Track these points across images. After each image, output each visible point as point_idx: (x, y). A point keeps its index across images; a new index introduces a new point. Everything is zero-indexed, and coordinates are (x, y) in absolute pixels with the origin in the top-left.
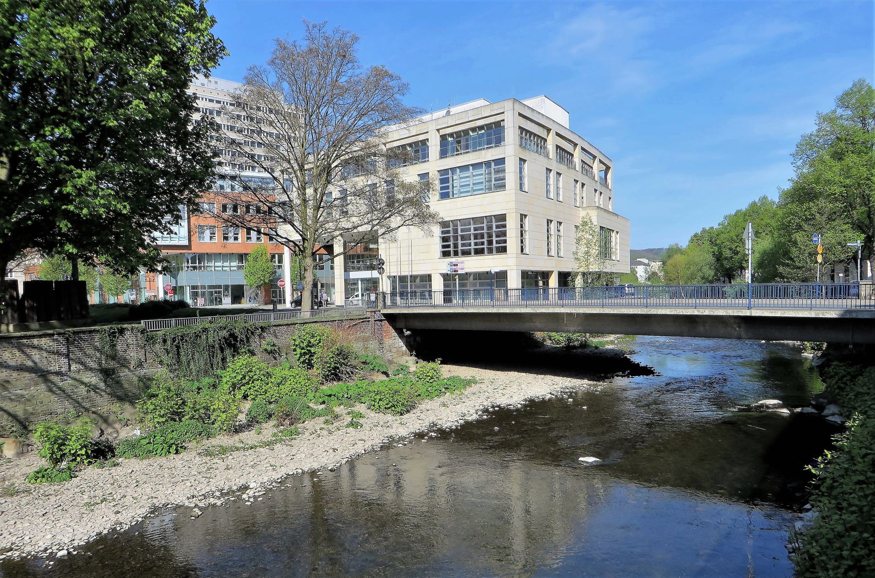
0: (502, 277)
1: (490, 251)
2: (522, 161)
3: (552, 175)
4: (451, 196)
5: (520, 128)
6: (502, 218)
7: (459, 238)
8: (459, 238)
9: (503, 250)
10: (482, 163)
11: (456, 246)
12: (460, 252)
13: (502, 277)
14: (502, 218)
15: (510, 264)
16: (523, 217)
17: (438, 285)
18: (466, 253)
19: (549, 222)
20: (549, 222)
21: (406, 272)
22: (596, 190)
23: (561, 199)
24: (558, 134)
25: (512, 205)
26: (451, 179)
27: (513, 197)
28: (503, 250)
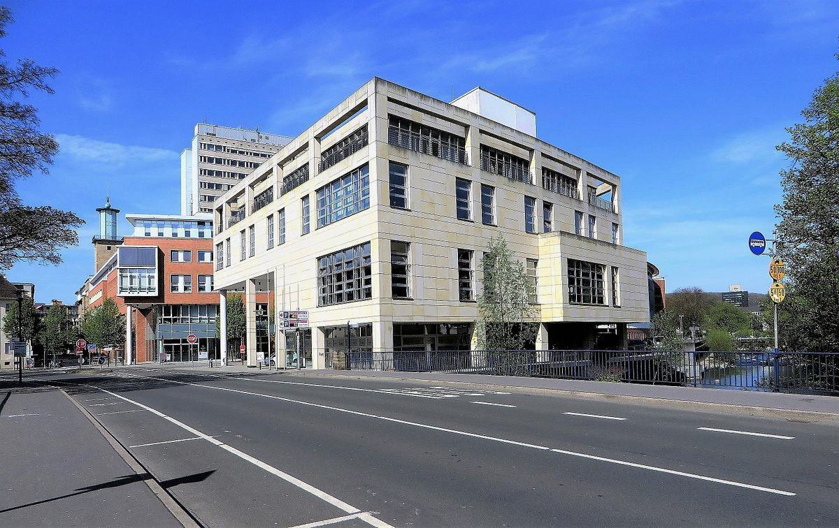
0: (367, 330)
3: (538, 208)
13: (367, 330)
19: (464, 255)
20: (464, 255)
24: (588, 174)
25: (375, 228)
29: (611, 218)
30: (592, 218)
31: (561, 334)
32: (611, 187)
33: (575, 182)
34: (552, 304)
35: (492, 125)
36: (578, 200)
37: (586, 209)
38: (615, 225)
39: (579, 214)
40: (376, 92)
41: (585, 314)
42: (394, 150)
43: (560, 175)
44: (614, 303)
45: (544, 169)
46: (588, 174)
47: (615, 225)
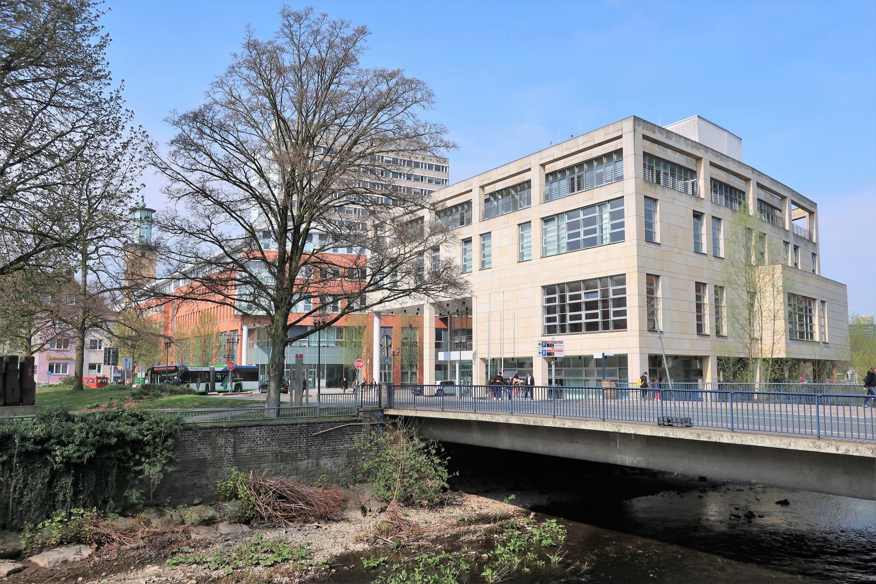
0: (621, 361)
1: (606, 327)
2: (651, 201)
3: (706, 221)
4: (599, 243)
5: (645, 154)
6: (620, 279)
7: (611, 303)
8: (611, 303)
9: (621, 325)
10: (594, 205)
11: (606, 315)
12: (568, 328)
13: (621, 361)
14: (620, 279)
15: (628, 343)
16: (652, 279)
17: (540, 374)
18: (576, 328)
19: (700, 286)
20: (700, 286)
21: (496, 356)
22: (786, 243)
23: (722, 255)
24: (712, 164)
25: (634, 262)
26: (598, 219)
27: (634, 251)
28: (621, 325)
29: (811, 249)
30: (796, 248)
31: (780, 368)
32: (807, 214)
33: (693, 173)
34: (773, 340)
35: (736, 165)
36: (699, 198)
37: (707, 209)
38: (814, 255)
39: (698, 216)
40: (635, 131)
41: (803, 351)
42: (647, 186)
43: (674, 165)
44: (718, 333)
45: (645, 154)
46: (712, 164)
47: (814, 255)
